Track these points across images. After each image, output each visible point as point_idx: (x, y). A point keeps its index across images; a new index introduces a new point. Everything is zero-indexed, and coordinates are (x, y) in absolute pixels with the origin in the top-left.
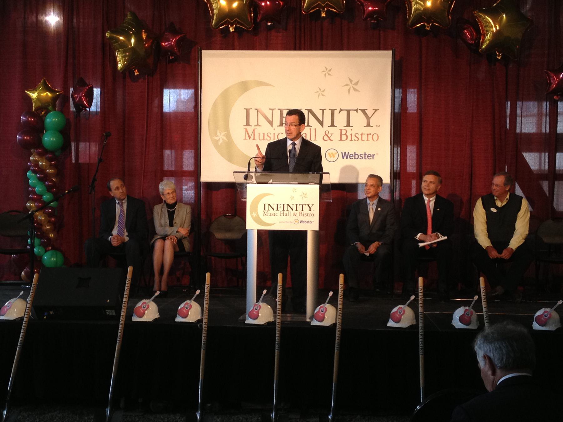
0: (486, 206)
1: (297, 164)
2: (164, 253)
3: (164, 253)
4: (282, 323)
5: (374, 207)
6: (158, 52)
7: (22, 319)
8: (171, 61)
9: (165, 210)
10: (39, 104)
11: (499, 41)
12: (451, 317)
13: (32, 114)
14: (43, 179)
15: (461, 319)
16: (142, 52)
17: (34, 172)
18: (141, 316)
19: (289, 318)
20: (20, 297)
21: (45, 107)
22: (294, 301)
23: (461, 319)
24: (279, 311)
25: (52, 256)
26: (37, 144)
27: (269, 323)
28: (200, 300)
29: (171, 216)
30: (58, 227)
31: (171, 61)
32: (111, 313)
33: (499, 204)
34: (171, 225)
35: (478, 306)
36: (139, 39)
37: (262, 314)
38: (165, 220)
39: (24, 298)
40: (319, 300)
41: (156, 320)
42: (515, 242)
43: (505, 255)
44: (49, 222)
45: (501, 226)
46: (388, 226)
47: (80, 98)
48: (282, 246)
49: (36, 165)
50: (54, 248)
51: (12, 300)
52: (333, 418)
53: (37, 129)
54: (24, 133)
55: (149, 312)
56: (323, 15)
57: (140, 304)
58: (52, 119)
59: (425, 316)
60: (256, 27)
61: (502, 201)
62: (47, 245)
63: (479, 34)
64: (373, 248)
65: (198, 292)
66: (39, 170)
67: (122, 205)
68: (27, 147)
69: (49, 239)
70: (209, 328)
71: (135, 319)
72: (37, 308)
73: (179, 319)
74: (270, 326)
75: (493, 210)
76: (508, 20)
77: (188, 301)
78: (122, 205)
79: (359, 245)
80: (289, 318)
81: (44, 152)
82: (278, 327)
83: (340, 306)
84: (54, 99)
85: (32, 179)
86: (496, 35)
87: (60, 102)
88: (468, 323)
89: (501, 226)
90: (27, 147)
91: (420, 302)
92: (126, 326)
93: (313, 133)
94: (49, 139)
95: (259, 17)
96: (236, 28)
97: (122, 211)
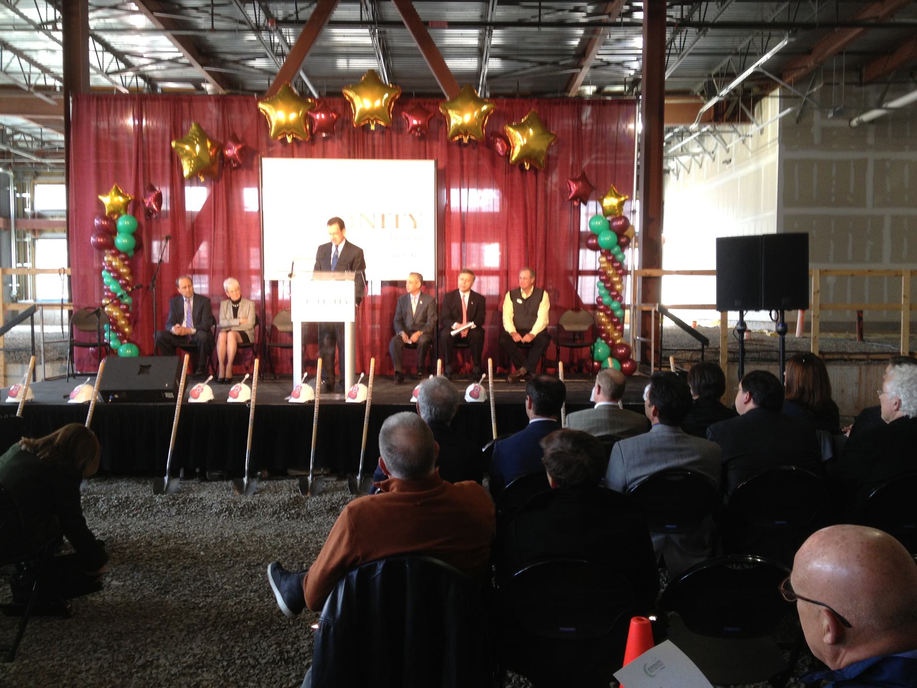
0: (513, 299)
1: (338, 263)
2: (227, 345)
3: (227, 345)
4: (320, 401)
5: (417, 301)
6: (224, 161)
7: (89, 402)
8: (235, 168)
9: (231, 305)
10: (112, 209)
11: (527, 154)
12: (464, 393)
13: (105, 218)
14: (118, 277)
15: (471, 394)
16: (207, 160)
17: (109, 271)
18: (196, 398)
19: (327, 397)
20: (88, 383)
21: (116, 212)
22: (334, 382)
23: (471, 394)
24: (318, 391)
25: (127, 348)
26: (111, 245)
27: (309, 402)
28: (249, 382)
29: (235, 311)
30: (133, 321)
31: (235, 168)
32: (169, 395)
33: (524, 296)
34: (235, 316)
35: (485, 383)
36: (203, 147)
37: (304, 392)
38: (231, 312)
39: (92, 383)
40: (355, 381)
41: (210, 401)
42: (537, 329)
43: (527, 338)
44: (124, 317)
45: (525, 315)
46: (429, 317)
47: (150, 203)
48: (324, 337)
49: (111, 265)
50: (129, 341)
51: (80, 386)
52: (361, 478)
53: (110, 231)
54: (99, 235)
55: (204, 393)
56: (373, 128)
57: (195, 387)
58: (124, 222)
59: (495, 394)
60: (313, 137)
61: (527, 293)
62: (123, 338)
63: (509, 146)
64: (415, 337)
65: (247, 376)
66: (114, 270)
67: (189, 302)
68: (101, 247)
69: (124, 333)
70: (257, 407)
71: (191, 400)
72: (104, 393)
73: (230, 400)
74: (311, 404)
75: (520, 301)
76: (535, 135)
77: (238, 384)
78: (189, 302)
79: (403, 335)
80: (327, 397)
81: (117, 253)
82: (317, 405)
83: (370, 386)
84: (126, 205)
85: (107, 277)
86: (523, 148)
87: (135, 207)
88: (477, 397)
89: (525, 315)
90: (101, 247)
91: (490, 381)
92: (182, 406)
93: (353, 236)
94: (121, 241)
95: (315, 129)
96: (293, 139)
97: (189, 307)
